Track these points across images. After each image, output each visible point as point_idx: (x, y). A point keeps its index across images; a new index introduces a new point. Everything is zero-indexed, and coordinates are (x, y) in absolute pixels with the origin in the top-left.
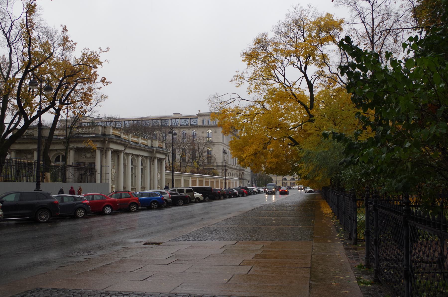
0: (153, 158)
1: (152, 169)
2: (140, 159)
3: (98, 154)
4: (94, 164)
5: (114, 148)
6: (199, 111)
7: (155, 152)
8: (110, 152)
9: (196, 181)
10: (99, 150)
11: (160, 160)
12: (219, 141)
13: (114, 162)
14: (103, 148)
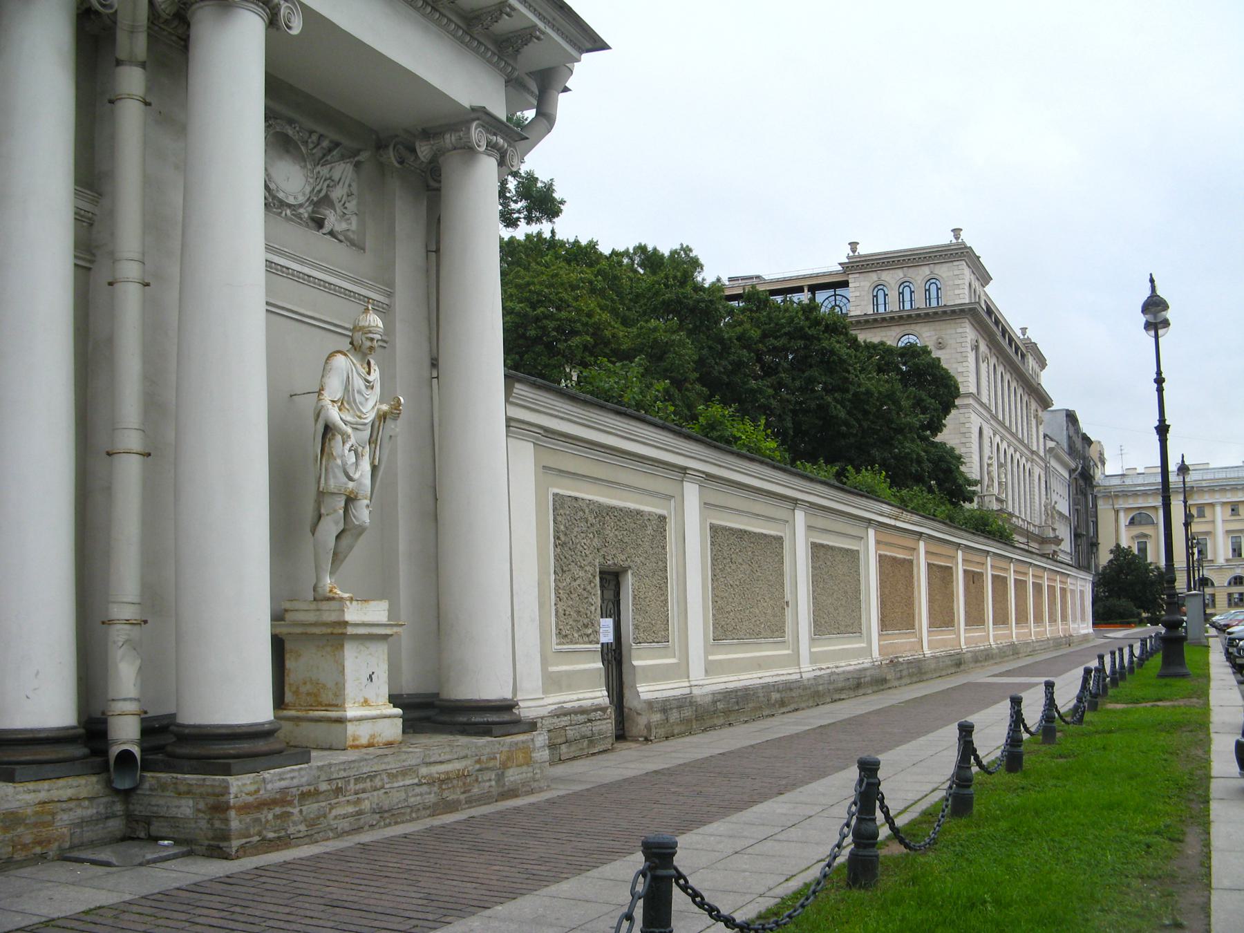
9: (908, 565)
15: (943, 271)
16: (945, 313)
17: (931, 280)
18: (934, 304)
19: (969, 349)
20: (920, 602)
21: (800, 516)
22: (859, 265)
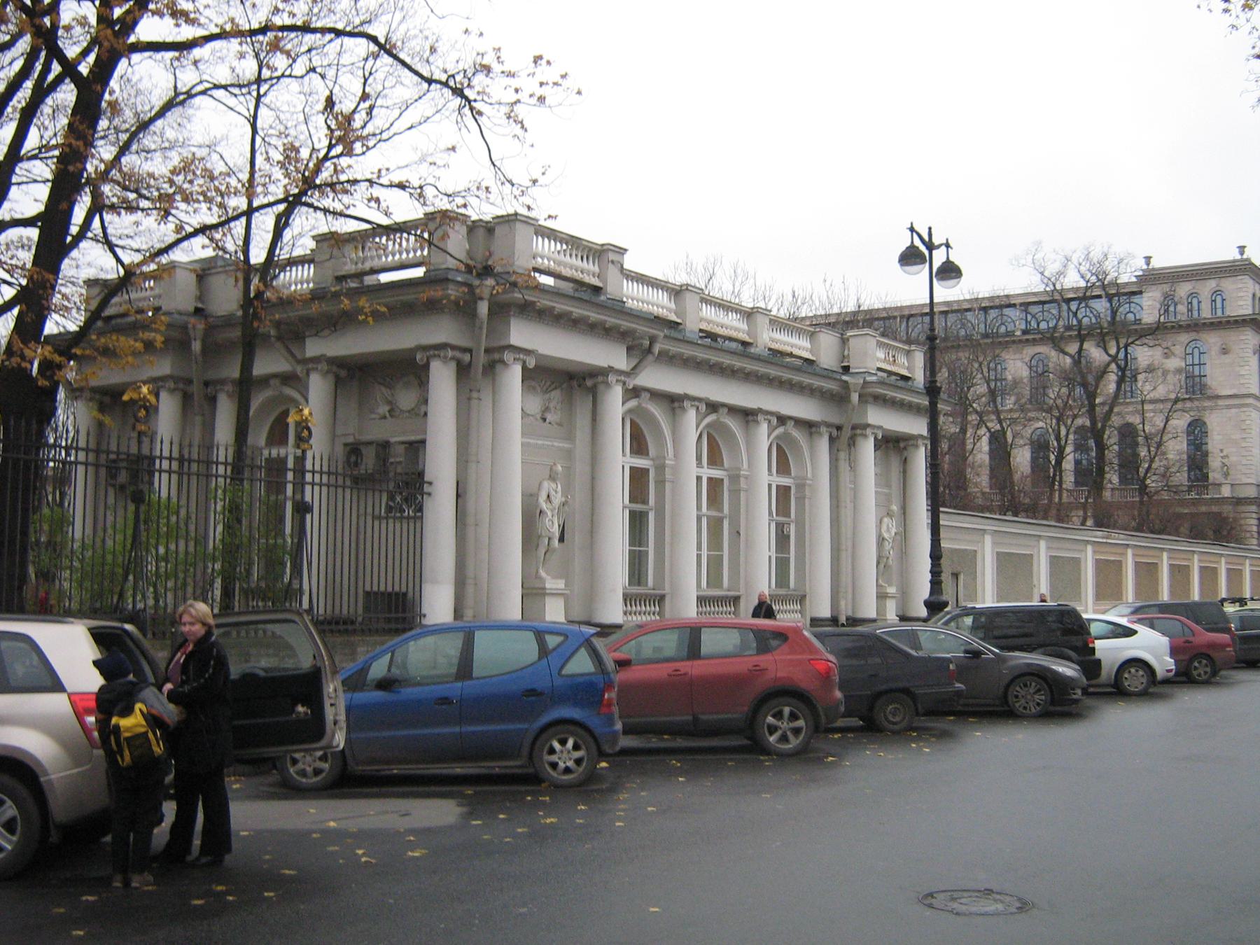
0: (847, 433)
1: (846, 496)
2: (763, 435)
3: (442, 380)
4: (417, 448)
5: (541, 351)
6: (1148, 259)
7: (855, 397)
8: (517, 370)
9: (1119, 565)
10: (445, 360)
11: (892, 444)
12: (1245, 391)
13: (889, 486)
14: (839, 428)
15: (1228, 285)
16: (1228, 322)
17: (1217, 292)
18: (1219, 313)
19: (1251, 354)
20: (1086, 595)
21: (1247, 562)
22: (1151, 277)
